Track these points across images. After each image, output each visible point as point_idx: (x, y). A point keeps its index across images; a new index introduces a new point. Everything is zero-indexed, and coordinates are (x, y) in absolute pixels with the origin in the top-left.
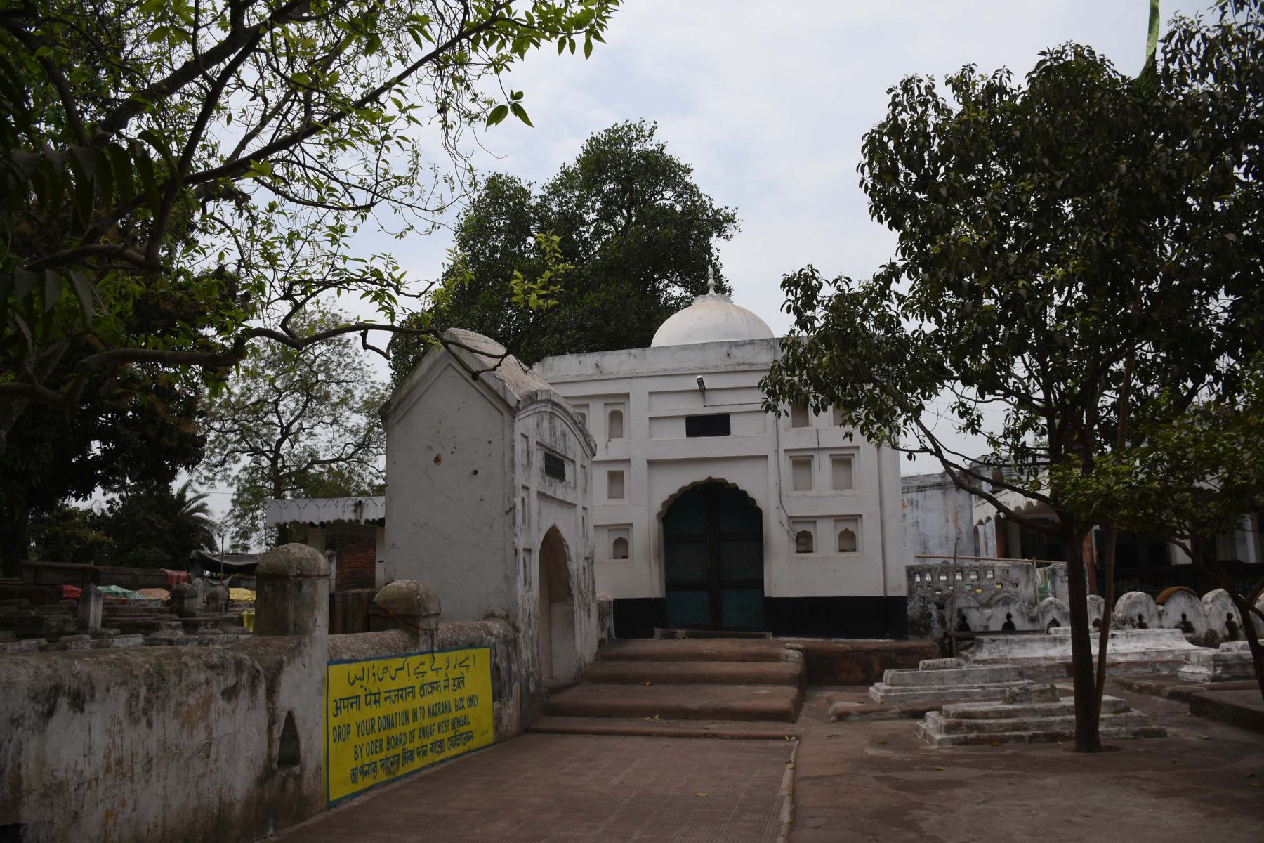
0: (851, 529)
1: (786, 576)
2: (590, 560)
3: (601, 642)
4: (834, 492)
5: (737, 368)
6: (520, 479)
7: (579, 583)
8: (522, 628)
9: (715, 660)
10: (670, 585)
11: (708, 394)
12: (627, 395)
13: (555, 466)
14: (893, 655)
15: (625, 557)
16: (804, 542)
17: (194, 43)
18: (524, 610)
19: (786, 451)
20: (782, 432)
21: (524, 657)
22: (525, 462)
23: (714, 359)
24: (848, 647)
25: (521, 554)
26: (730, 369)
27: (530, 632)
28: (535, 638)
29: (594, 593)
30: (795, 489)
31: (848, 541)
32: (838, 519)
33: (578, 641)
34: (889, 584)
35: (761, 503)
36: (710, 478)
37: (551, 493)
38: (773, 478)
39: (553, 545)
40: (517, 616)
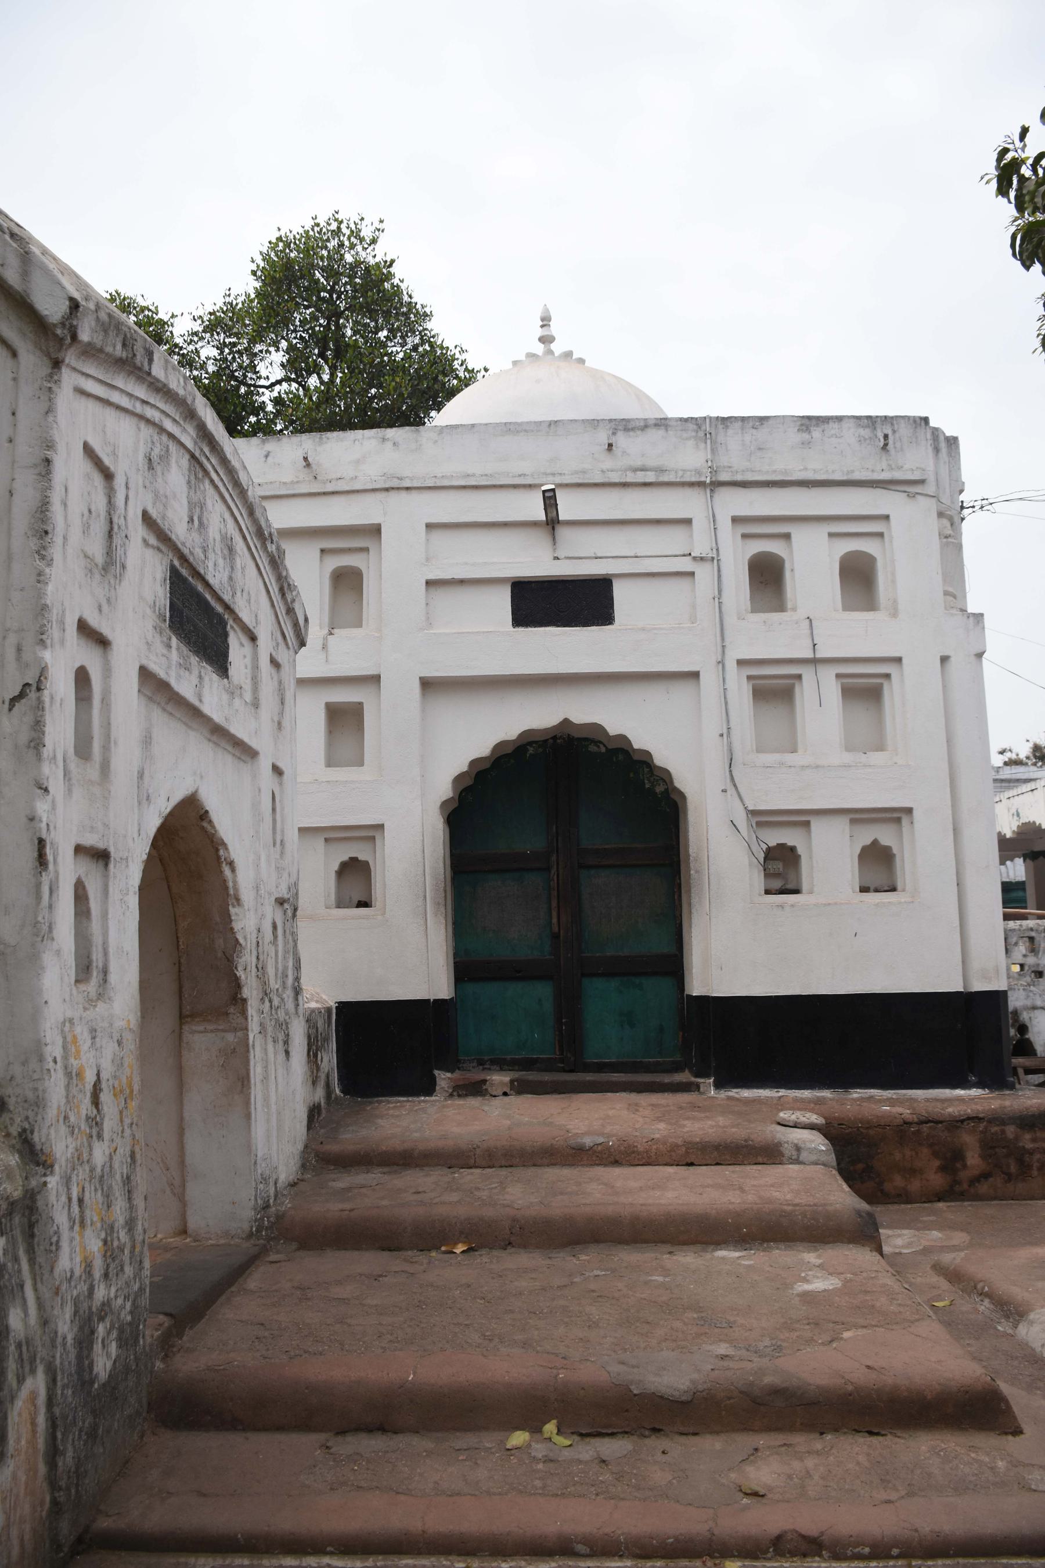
0: (885, 841)
1: (741, 946)
2: (287, 904)
3: (314, 1112)
4: (848, 758)
5: (630, 478)
6: (70, 591)
7: (261, 969)
8: (61, 1146)
9: (616, 1163)
10: (465, 970)
11: (562, 532)
12: (376, 531)
13: (199, 620)
14: (1011, 1131)
15: (364, 904)
16: (782, 870)
17: (529, 1446)
18: (73, 1076)
19: (741, 663)
20: (730, 620)
21: (67, 1261)
22: (97, 549)
23: (576, 457)
24: (906, 1112)
25: (66, 868)
26: (615, 478)
27: (99, 1154)
28: (120, 1168)
29: (297, 991)
30: (759, 750)
31: (879, 869)
32: (859, 817)
33: (259, 1130)
34: (975, 964)
35: (684, 779)
36: (566, 722)
37: (185, 688)
38: (712, 724)
39: (186, 856)
40: (38, 1103)
